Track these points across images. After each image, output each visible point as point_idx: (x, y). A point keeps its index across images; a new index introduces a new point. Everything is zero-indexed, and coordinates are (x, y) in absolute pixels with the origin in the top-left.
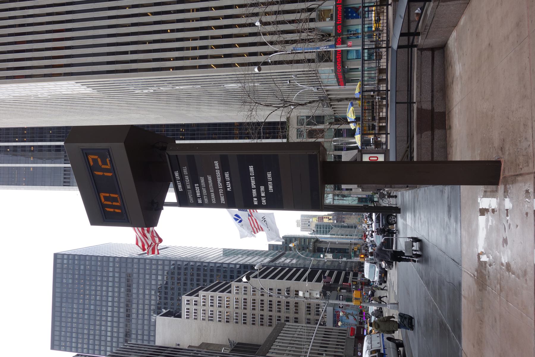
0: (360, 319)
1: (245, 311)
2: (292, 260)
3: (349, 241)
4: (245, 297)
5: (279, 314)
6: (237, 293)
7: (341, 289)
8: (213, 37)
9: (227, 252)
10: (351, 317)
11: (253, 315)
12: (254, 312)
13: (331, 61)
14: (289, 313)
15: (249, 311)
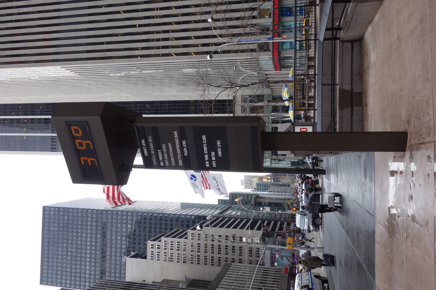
0: (293, 260)
1: (199, 254)
2: (237, 212)
3: (283, 197)
4: (199, 242)
5: (226, 256)
6: (192, 239)
7: (277, 236)
8: (173, 31)
9: (184, 206)
10: (285, 259)
11: (205, 256)
12: (206, 254)
13: (270, 51)
14: (234, 255)
15: (202, 254)
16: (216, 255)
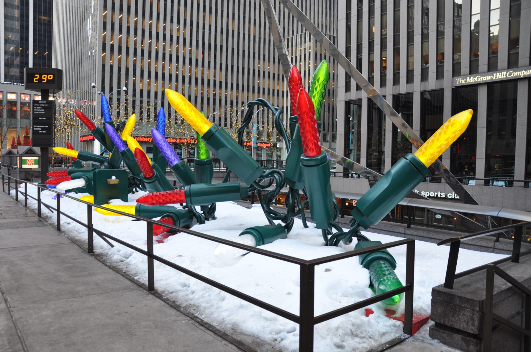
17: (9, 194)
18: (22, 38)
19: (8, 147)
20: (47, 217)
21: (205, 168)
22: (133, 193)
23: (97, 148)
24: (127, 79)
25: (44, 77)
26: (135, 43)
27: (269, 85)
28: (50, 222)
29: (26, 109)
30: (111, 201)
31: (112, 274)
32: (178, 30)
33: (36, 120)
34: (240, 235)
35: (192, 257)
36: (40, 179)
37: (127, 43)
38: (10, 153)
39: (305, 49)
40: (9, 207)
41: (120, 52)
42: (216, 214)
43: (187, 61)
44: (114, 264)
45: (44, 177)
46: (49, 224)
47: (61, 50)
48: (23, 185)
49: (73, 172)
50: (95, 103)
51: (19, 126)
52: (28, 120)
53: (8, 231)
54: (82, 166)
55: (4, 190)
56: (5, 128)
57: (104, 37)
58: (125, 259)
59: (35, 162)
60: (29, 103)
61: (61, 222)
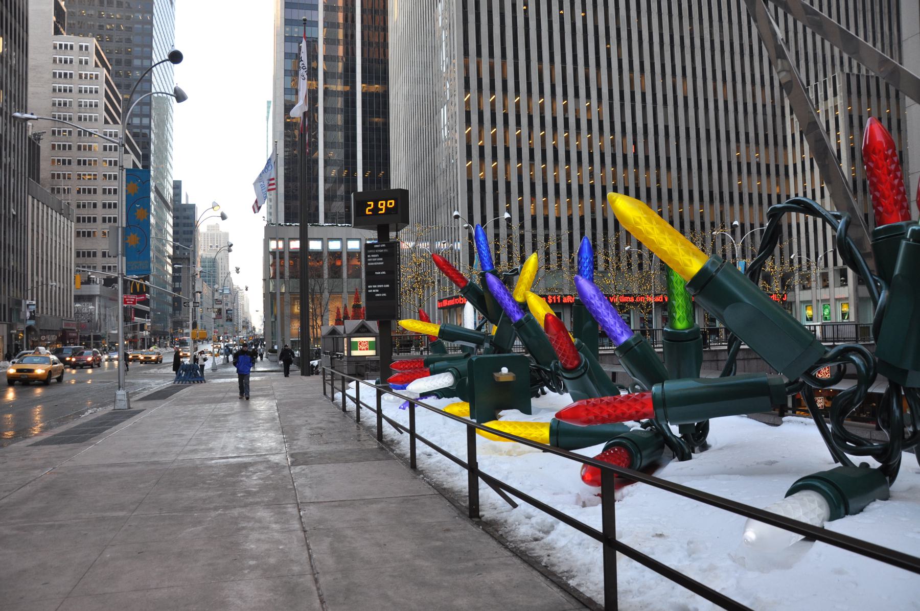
1: (74, 148)
12: (74, 163)
16: (100, 199)
17: (333, 399)
18: (346, 156)
19: (331, 323)
20: (392, 441)
21: (687, 348)
22: (538, 396)
23: (469, 317)
24: (508, 200)
25: (382, 205)
26: (519, 138)
27: (760, 186)
28: (398, 451)
29: (355, 262)
30: (502, 413)
31: (520, 572)
32: (589, 108)
33: (371, 278)
34: (790, 493)
35: (689, 543)
36: (379, 373)
37: (505, 142)
38: (333, 332)
39: (827, 111)
40: (333, 422)
41: (495, 157)
42: (710, 439)
43: (608, 160)
44: (523, 546)
45: (387, 372)
46: (396, 454)
47: (403, 166)
48: (353, 384)
49: (433, 361)
50: (458, 246)
51: (345, 290)
52: (358, 280)
53: (331, 467)
54: (444, 351)
55: (325, 394)
56: (326, 294)
57: (469, 136)
58: (541, 535)
59: (371, 346)
60: (360, 253)
61: (418, 452)
